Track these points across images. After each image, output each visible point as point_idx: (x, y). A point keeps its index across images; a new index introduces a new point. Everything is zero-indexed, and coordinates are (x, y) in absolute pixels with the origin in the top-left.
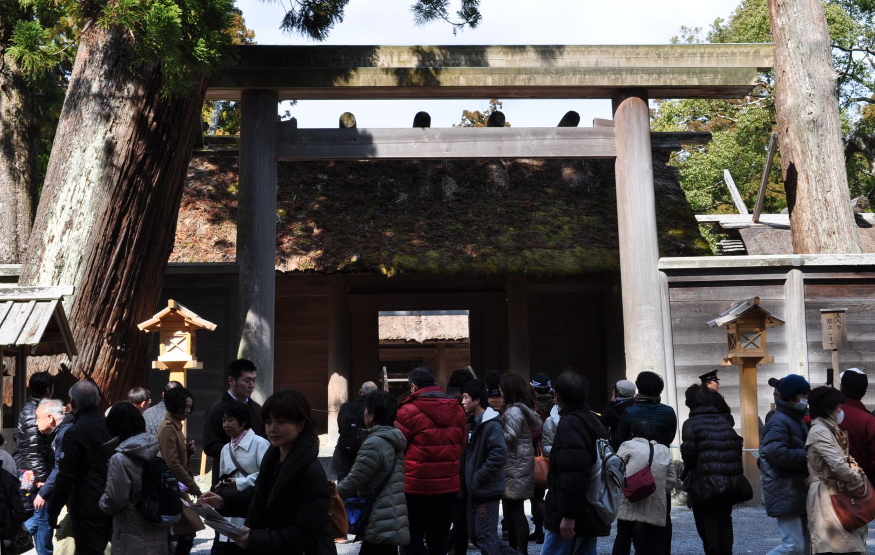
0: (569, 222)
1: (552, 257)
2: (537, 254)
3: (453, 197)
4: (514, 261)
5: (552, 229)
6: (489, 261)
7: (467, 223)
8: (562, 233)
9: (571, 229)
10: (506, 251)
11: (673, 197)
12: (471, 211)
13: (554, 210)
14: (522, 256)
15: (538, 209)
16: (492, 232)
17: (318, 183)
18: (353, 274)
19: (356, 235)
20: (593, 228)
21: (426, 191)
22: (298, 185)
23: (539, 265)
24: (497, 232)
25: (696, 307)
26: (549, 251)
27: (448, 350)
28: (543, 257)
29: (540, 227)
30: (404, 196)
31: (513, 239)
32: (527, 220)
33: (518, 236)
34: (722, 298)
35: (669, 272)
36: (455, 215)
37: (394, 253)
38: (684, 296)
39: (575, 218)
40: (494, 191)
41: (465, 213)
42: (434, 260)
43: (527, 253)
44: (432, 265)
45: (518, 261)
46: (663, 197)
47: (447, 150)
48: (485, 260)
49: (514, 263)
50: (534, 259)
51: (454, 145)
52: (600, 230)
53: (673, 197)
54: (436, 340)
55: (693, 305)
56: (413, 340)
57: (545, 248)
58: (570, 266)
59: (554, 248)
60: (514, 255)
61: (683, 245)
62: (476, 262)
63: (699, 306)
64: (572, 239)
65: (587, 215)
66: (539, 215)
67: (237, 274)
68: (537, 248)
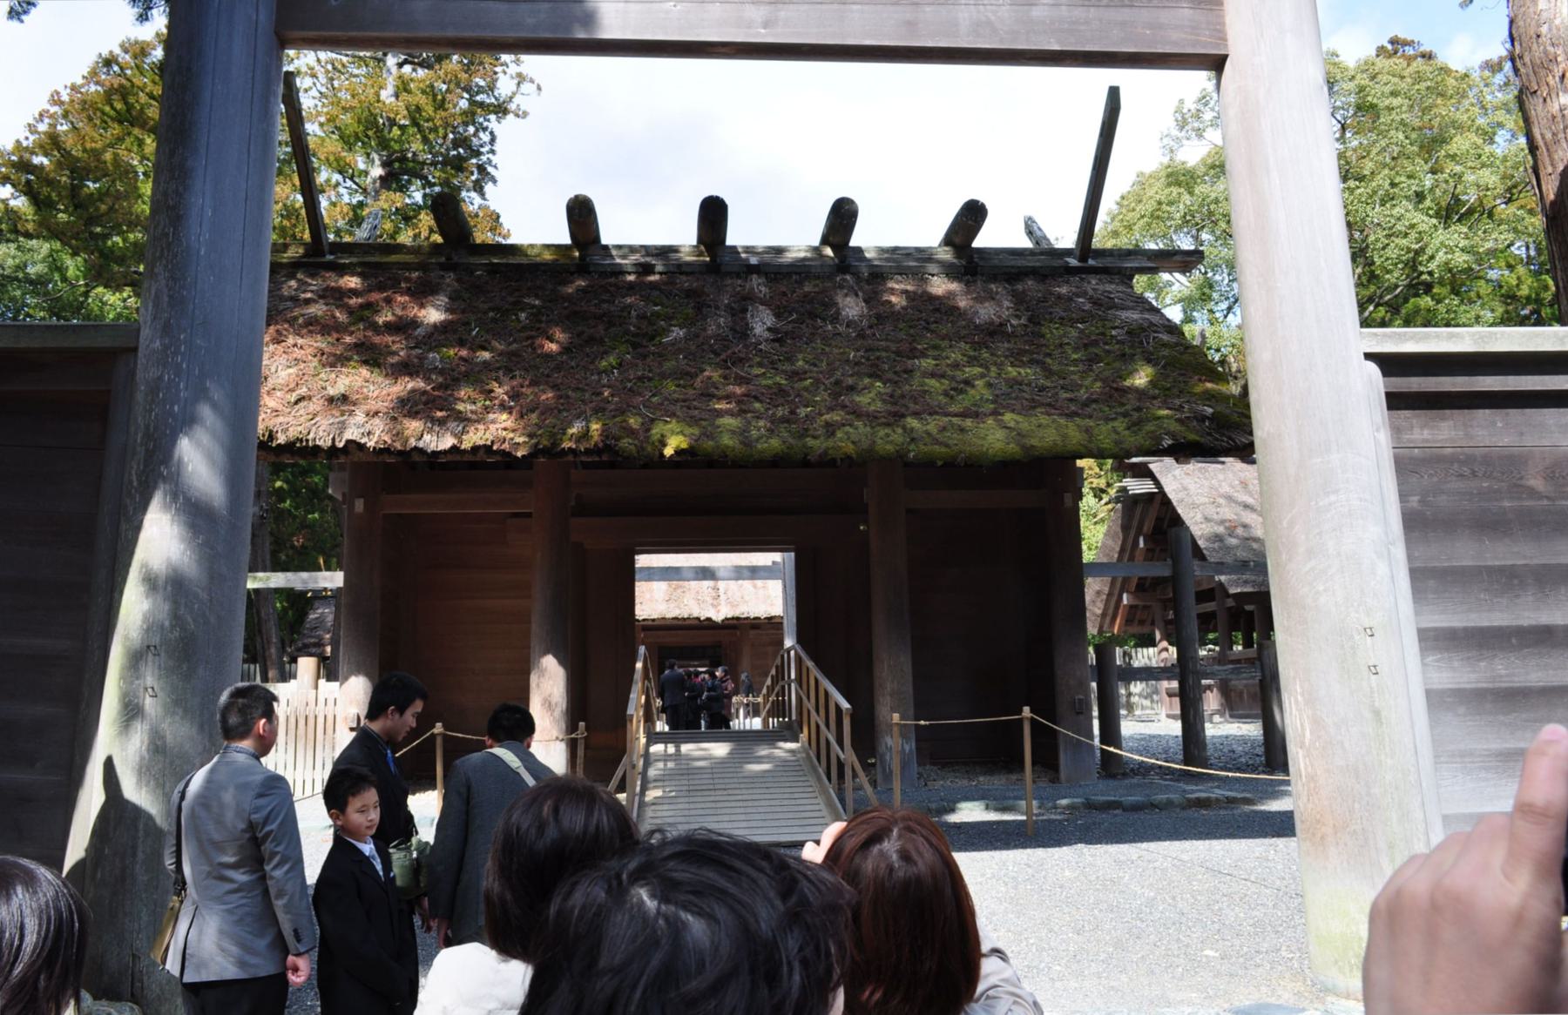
0: (982, 376)
1: (962, 430)
2: (933, 425)
3: (767, 334)
4: (888, 435)
5: (954, 385)
6: (839, 434)
7: (796, 375)
8: (972, 392)
9: (989, 385)
10: (872, 418)
11: (1165, 337)
12: (800, 356)
13: (955, 356)
14: (904, 428)
15: (924, 355)
16: (840, 390)
17: (522, 310)
18: (570, 458)
19: (583, 390)
20: (1029, 385)
21: (719, 326)
22: (485, 313)
23: (938, 442)
24: (852, 388)
25: (1462, 463)
26: (955, 420)
27: (752, 632)
28: (944, 429)
29: (932, 382)
30: (677, 333)
31: (884, 401)
32: (906, 371)
33: (892, 396)
34: (1529, 441)
35: (1389, 364)
36: (772, 363)
37: (653, 420)
38: (1426, 434)
39: (993, 369)
40: (841, 329)
41: (790, 359)
42: (733, 432)
43: (913, 422)
44: (727, 441)
45: (897, 436)
46: (1147, 337)
47: (766, 25)
48: (833, 434)
49: (888, 440)
50: (929, 434)
51: (785, 12)
52: (1042, 389)
53: (1165, 337)
54: (738, 619)
55: (1452, 460)
56: (709, 619)
57: (947, 415)
58: (999, 445)
59: (964, 415)
60: (888, 425)
61: (1210, 410)
62: (815, 437)
63: (1469, 460)
64: (994, 402)
65: (1013, 365)
66: (927, 363)
67: (135, 350)
68: (930, 414)
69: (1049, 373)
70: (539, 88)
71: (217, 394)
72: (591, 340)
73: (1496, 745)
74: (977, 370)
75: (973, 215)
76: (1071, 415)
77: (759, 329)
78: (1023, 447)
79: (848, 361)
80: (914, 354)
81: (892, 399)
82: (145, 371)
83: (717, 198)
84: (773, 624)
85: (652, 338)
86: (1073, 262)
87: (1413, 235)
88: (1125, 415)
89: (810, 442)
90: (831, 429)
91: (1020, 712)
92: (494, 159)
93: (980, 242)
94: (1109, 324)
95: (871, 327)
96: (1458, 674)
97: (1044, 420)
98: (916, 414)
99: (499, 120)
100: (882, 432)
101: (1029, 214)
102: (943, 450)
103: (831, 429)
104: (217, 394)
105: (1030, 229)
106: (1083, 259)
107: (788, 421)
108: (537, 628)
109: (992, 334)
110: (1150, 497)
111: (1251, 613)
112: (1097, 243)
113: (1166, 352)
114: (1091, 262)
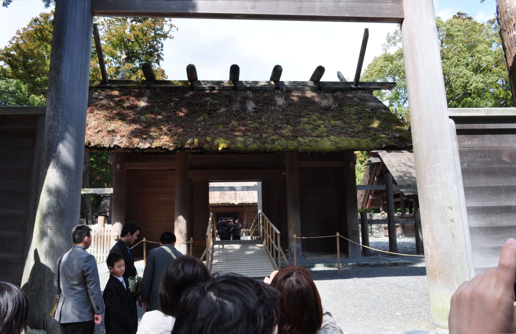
0: (323, 124)
1: (317, 141)
2: (307, 140)
3: (252, 110)
4: (292, 143)
5: (314, 127)
6: (276, 143)
7: (262, 123)
8: (320, 129)
9: (326, 127)
10: (287, 138)
11: (383, 111)
12: (263, 117)
13: (314, 117)
14: (298, 141)
15: (304, 117)
16: (277, 128)
17: (172, 102)
18: (188, 151)
19: (192, 128)
20: (339, 127)
21: (237, 107)
22: (160, 103)
23: (309, 146)
24: (280, 128)
25: (481, 152)
26: (314, 138)
27: (248, 208)
28: (311, 141)
29: (307, 126)
30: (223, 109)
31: (291, 132)
32: (298, 122)
33: (293, 130)
34: (503, 145)
35: (457, 120)
36: (254, 119)
37: (215, 138)
38: (469, 143)
39: (327, 121)
40: (277, 108)
41: (260, 118)
42: (241, 142)
43: (300, 139)
44: (239, 145)
45: (295, 143)
46: (378, 111)
47: (252, 8)
48: (274, 143)
49: (292, 145)
50: (306, 143)
51: (258, 4)
52: (343, 128)
53: (383, 111)
54: (243, 204)
55: (478, 151)
56: (233, 204)
57: (312, 136)
58: (329, 147)
59: (317, 136)
60: (292, 140)
61: (398, 135)
62: (268, 144)
63: (483, 151)
64: (327, 132)
65: (333, 120)
66: (305, 120)
67: (44, 115)
68: (306, 136)
69: (345, 123)
70: (177, 29)
71: (71, 130)
72: (195, 112)
73: (492, 245)
74: (322, 122)
75: (320, 71)
76: (353, 137)
77: (250, 108)
78: (337, 147)
79: (279, 119)
80: (301, 116)
81: (294, 131)
82: (48, 122)
83: (236, 65)
84: (254, 205)
85: (215, 111)
86: (353, 86)
87: (465, 77)
88: (370, 137)
89: (267, 145)
90: (273, 141)
91: (336, 234)
92: (163, 52)
93: (322, 80)
94: (365, 107)
95: (286, 108)
96: (480, 222)
97: (344, 138)
98: (301, 136)
99: (164, 39)
100: (290, 142)
101: (338, 70)
102: (310, 148)
103: (273, 141)
104: (71, 130)
105: (339, 75)
106: (356, 85)
107: (259, 139)
108: (177, 207)
109: (326, 110)
110: (378, 163)
111: (412, 202)
112: (361, 80)
113: (384, 116)
114: (359, 86)
